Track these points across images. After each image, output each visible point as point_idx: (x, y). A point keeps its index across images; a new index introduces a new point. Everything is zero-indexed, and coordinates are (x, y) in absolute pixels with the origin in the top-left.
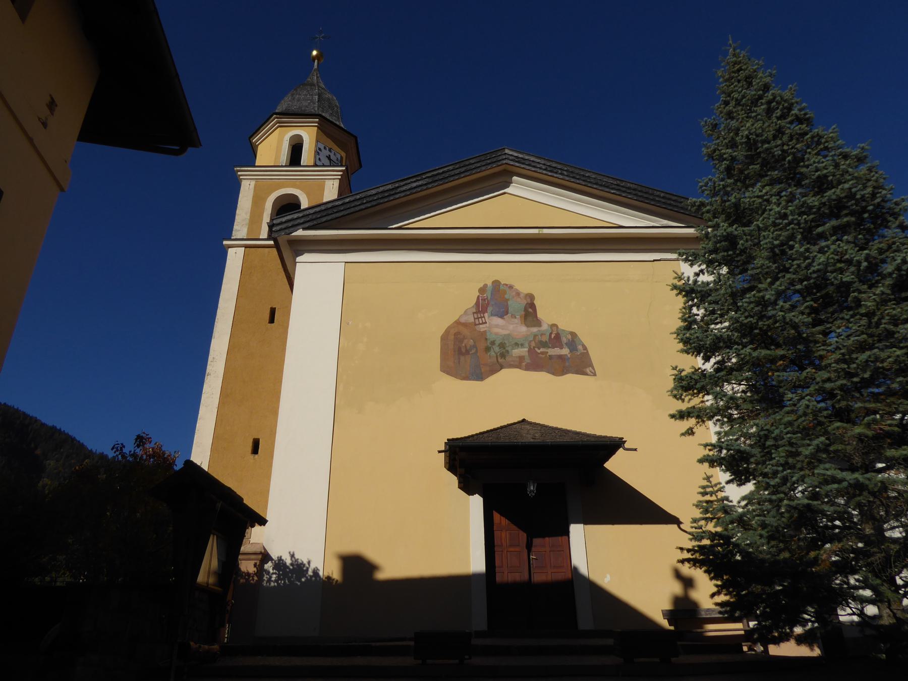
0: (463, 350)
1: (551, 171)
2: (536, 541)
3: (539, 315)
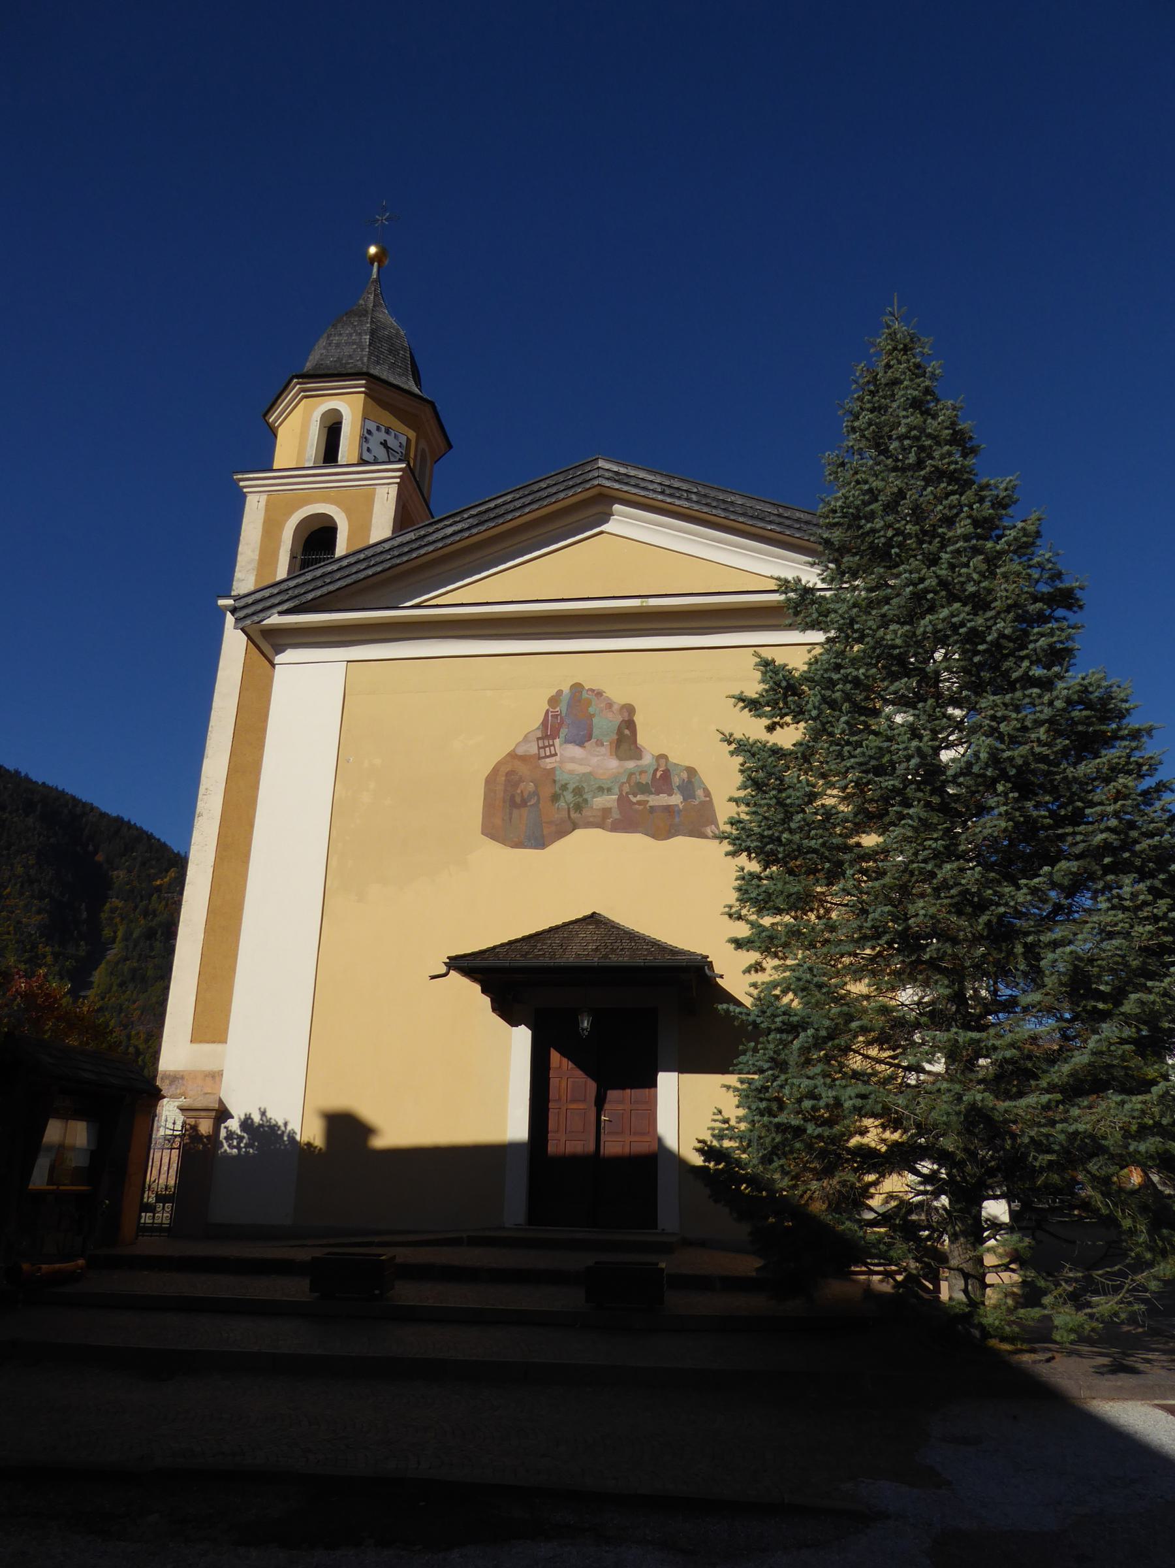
0: (518, 800)
1: (671, 495)
2: (612, 1095)
3: (641, 740)
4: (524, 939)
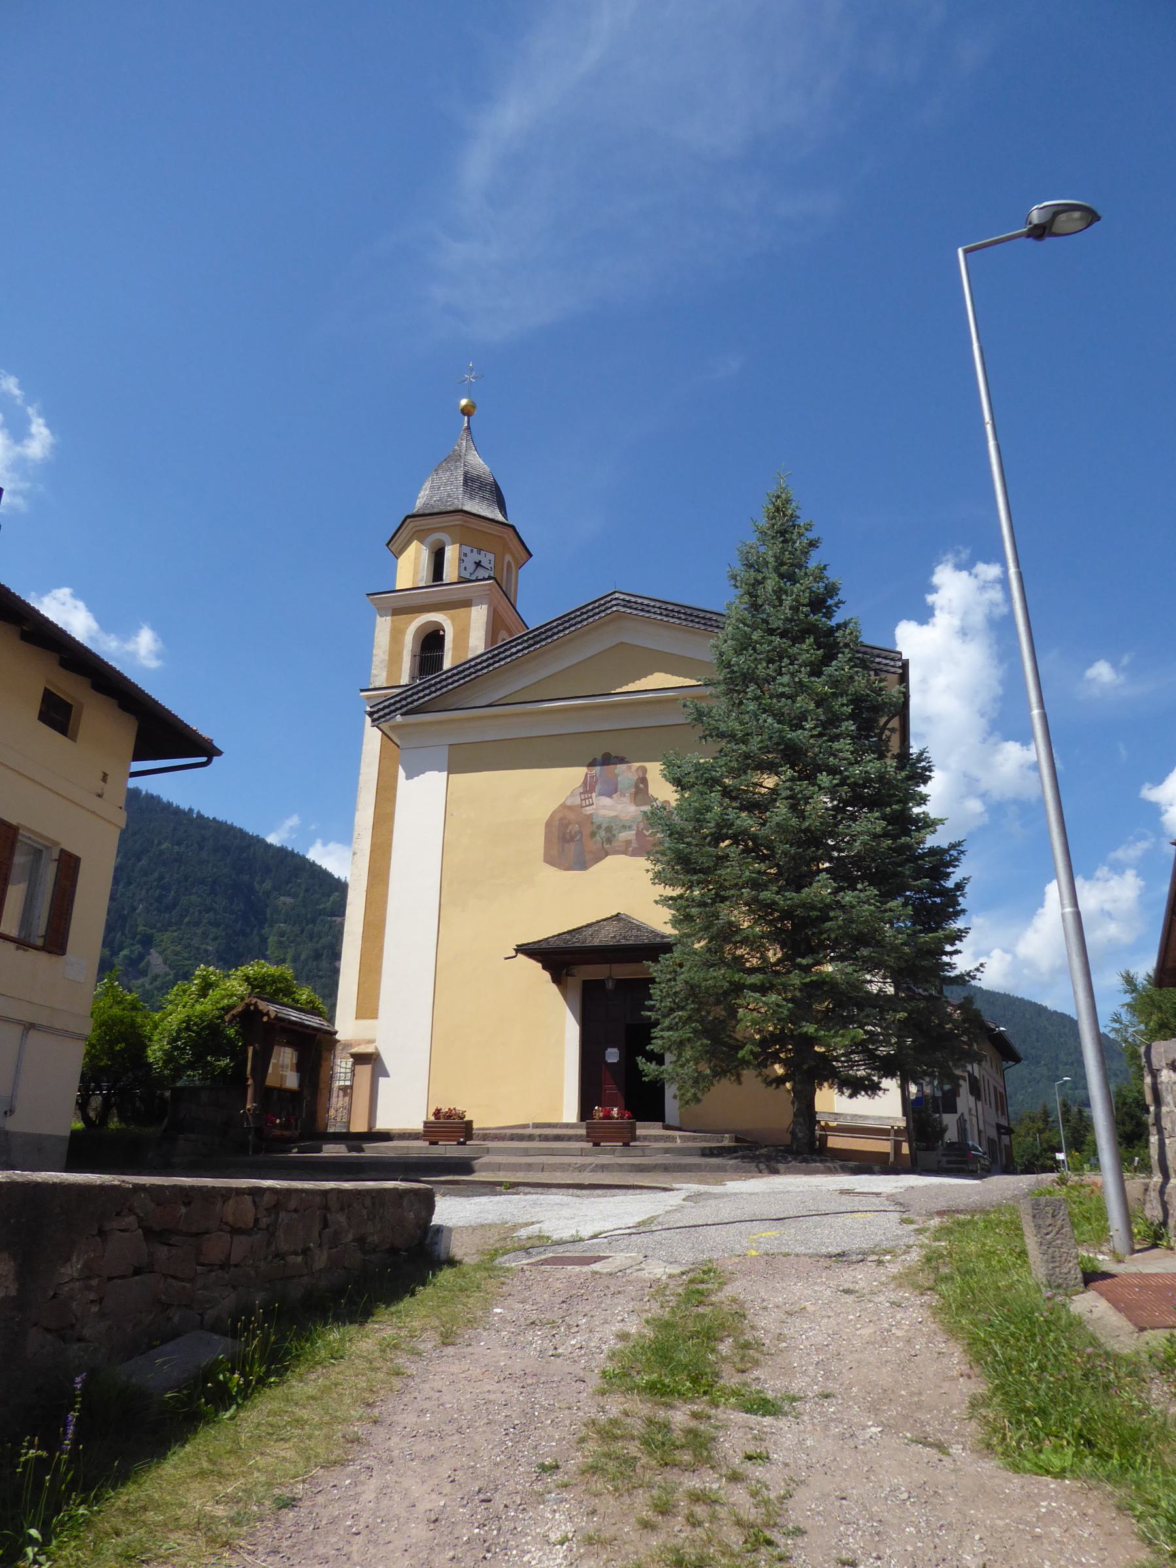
0: (568, 836)
4: (568, 932)
